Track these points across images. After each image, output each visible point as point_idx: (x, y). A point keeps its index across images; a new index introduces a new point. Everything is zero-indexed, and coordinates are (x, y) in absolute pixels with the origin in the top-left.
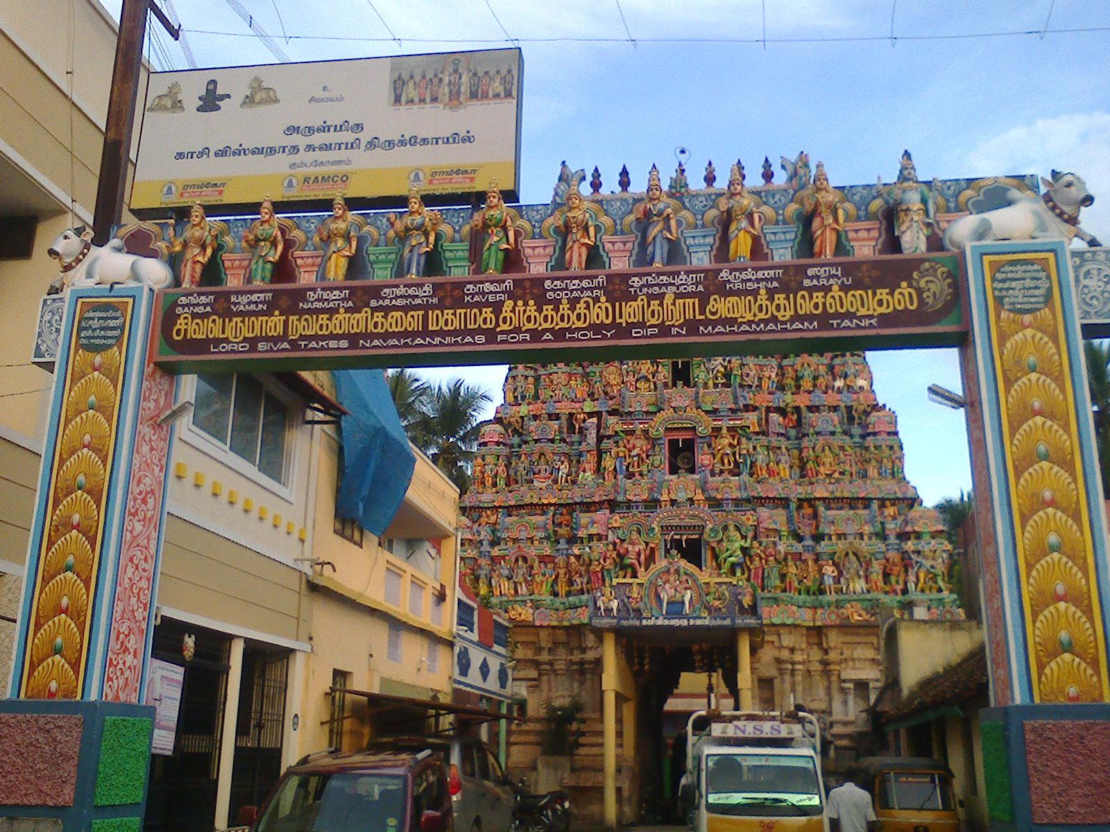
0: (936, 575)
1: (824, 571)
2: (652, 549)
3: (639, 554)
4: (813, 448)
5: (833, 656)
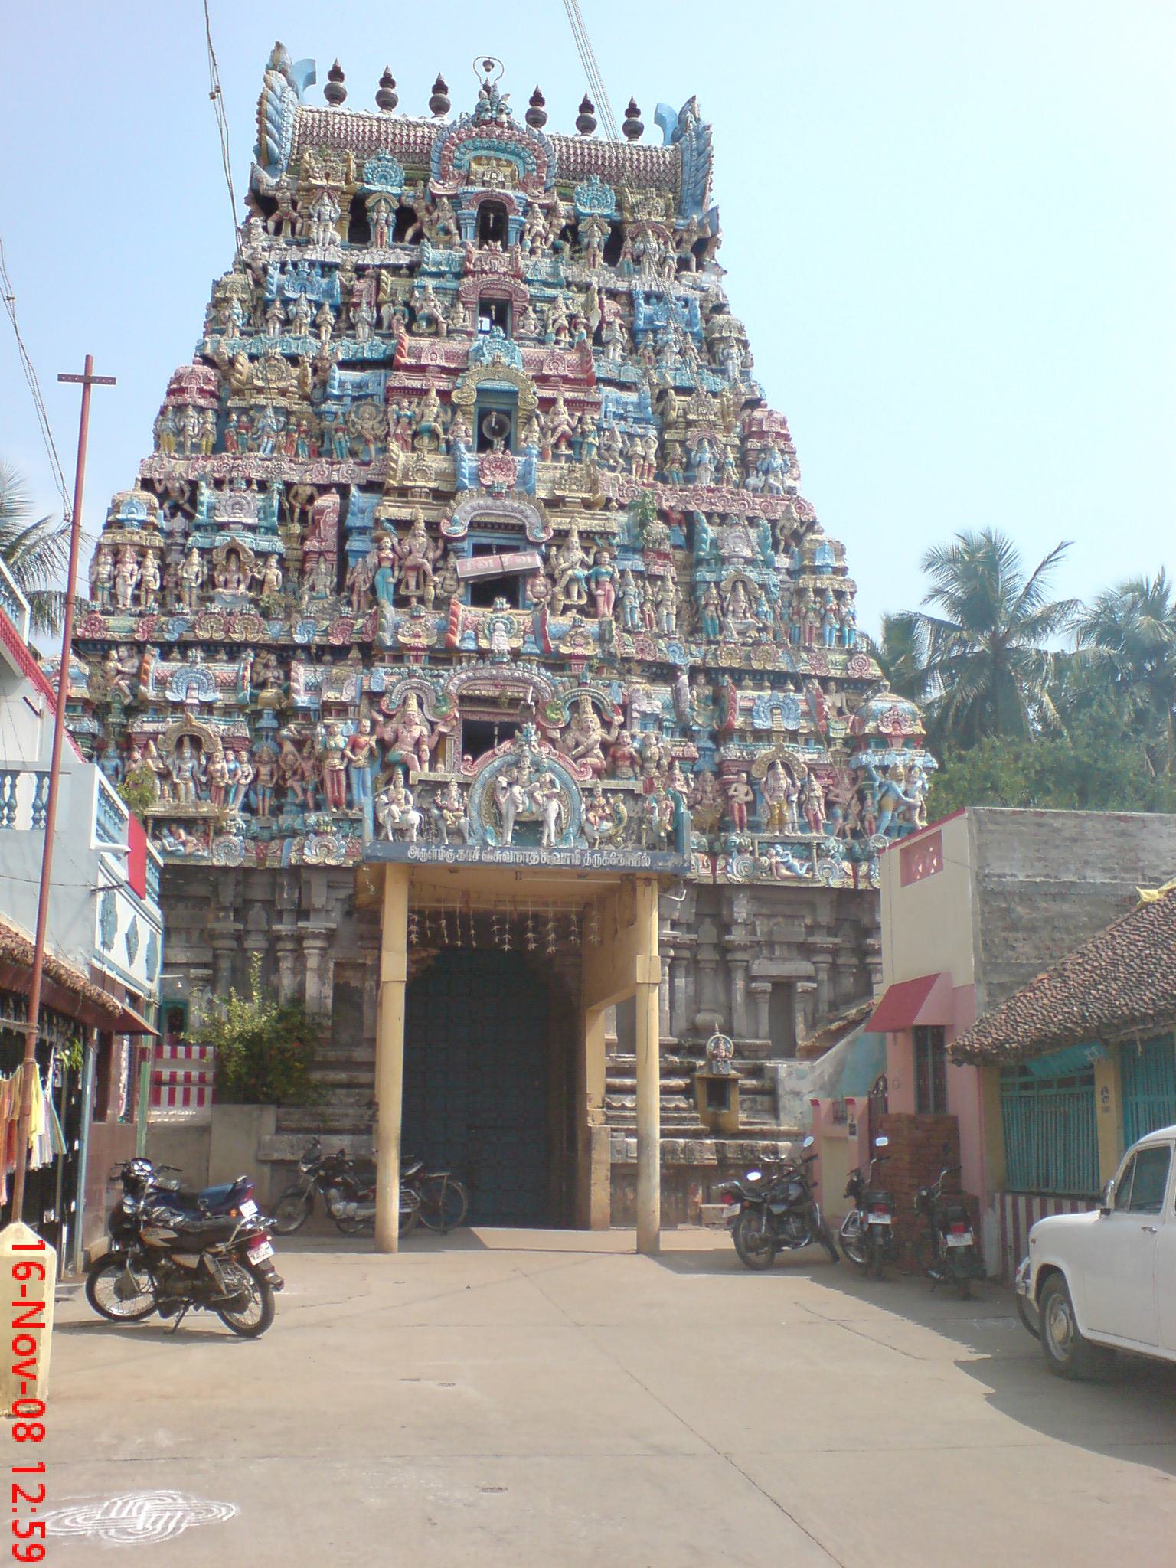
0: (911, 808)
1: (731, 792)
2: (443, 736)
3: (418, 743)
4: (717, 584)
5: (737, 936)
